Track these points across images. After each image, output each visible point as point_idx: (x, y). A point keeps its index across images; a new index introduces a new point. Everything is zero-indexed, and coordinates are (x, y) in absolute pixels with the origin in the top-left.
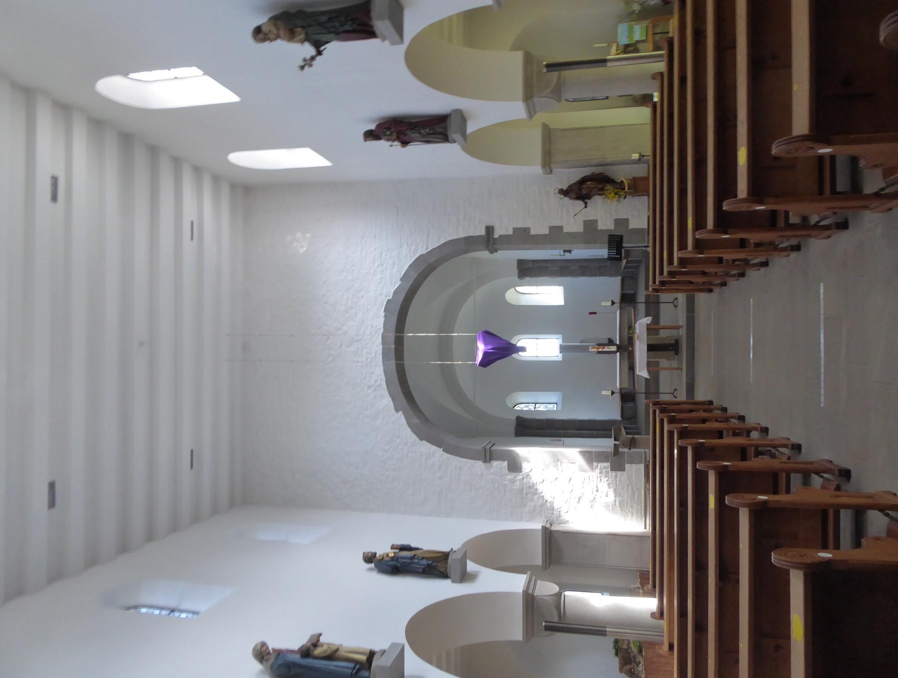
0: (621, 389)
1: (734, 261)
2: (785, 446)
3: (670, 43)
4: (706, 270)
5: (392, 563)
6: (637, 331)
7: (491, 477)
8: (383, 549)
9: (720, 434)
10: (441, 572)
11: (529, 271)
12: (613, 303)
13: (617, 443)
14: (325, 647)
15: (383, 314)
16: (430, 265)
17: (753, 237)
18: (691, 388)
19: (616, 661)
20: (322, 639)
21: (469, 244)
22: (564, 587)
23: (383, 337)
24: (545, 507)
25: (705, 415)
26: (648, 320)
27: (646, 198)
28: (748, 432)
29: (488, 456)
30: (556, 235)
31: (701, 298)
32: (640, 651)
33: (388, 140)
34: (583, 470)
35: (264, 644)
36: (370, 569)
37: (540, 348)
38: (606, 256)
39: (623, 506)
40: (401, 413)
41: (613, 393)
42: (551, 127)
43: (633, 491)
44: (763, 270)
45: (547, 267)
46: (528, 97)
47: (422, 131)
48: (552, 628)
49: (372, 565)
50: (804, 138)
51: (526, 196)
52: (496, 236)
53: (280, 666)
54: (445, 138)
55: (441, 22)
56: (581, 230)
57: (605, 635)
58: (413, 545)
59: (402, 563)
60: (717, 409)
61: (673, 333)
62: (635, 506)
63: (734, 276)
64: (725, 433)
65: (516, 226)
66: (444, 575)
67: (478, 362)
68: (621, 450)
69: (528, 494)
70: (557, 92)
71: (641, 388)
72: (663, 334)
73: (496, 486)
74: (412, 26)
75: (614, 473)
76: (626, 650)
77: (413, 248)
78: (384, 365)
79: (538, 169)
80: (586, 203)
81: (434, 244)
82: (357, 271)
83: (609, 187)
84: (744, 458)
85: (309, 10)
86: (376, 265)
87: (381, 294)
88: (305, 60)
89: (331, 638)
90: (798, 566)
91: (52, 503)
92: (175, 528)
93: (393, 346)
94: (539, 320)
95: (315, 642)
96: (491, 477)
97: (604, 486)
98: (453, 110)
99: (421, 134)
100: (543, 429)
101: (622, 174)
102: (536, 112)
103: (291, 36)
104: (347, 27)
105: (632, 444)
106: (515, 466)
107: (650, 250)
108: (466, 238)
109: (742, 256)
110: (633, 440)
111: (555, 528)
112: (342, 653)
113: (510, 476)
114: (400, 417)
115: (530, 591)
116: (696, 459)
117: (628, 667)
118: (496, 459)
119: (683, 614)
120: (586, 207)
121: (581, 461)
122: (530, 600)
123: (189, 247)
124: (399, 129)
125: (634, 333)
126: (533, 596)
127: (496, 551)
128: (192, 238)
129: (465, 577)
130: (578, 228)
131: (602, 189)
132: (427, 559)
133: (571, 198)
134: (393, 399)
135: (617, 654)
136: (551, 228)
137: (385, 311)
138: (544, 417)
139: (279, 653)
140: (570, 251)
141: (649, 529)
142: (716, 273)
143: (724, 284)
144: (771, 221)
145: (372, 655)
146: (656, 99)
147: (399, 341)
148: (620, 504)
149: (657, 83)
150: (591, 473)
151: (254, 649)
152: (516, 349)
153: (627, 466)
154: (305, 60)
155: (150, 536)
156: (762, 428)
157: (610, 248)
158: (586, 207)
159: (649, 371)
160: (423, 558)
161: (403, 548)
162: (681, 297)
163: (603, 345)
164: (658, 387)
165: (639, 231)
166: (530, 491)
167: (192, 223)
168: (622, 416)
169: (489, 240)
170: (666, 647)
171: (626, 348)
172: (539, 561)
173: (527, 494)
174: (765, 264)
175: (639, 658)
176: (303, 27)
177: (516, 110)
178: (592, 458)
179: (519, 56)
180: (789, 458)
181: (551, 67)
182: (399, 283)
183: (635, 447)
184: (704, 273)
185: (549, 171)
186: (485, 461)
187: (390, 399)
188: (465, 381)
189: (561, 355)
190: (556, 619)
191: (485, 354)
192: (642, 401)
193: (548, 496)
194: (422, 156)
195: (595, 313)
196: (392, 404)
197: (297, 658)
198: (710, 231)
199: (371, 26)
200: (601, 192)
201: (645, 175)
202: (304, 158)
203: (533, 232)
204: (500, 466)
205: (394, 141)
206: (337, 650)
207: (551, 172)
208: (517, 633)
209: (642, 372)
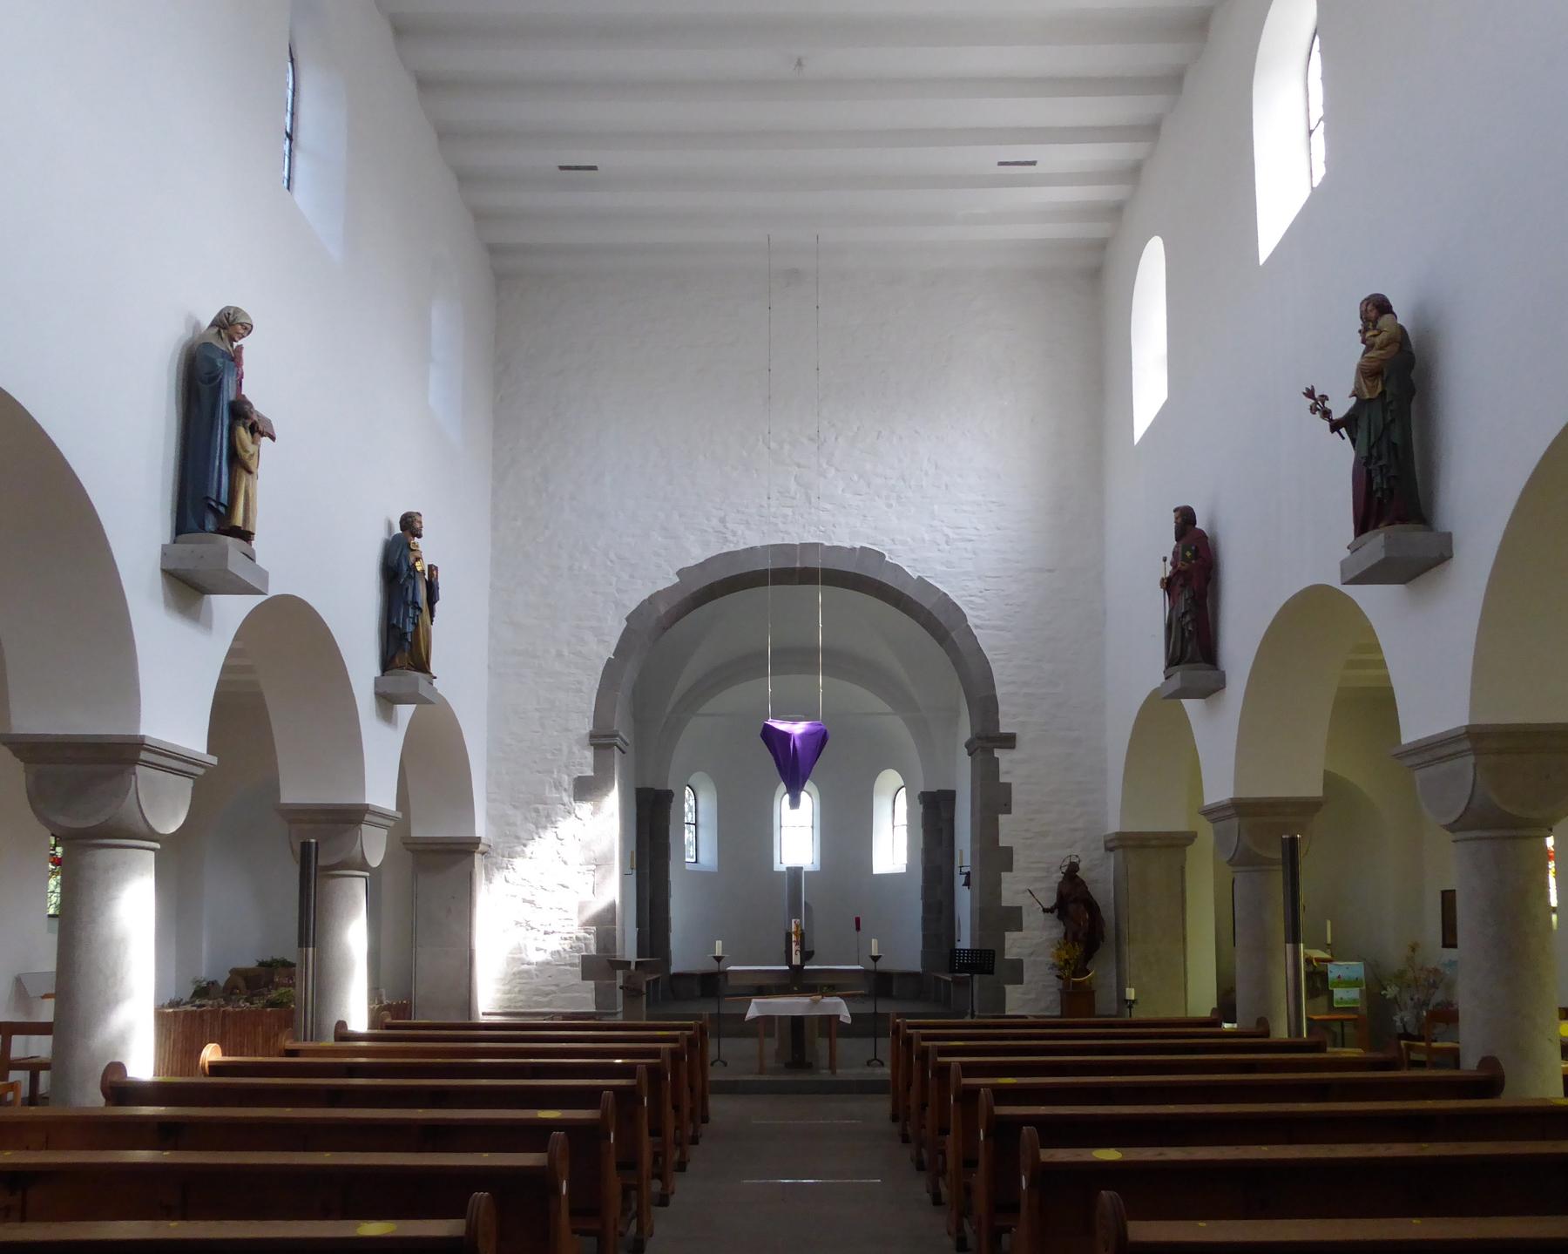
0: (726, 973)
1: (943, 1153)
2: (640, 1229)
3: (1318, 1047)
4: (928, 1109)
5: (405, 568)
6: (827, 1000)
7: (565, 749)
8: (429, 550)
9: (656, 1131)
10: (393, 657)
11: (934, 812)
12: (875, 959)
13: (633, 967)
14: (251, 448)
15: (857, 546)
16: (947, 633)
17: (979, 1179)
18: (731, 1088)
19: (249, 962)
20: (265, 441)
21: (984, 704)
22: (177, 864)
23: (816, 545)
24: (514, 842)
25: (686, 1111)
26: (845, 1015)
27: (1058, 1013)
28: (659, 1176)
29: (601, 741)
30: (995, 858)
31: (881, 1106)
32: (272, 1004)
33: (1175, 553)
34: (581, 909)
35: (248, 329)
36: (390, 527)
37: (797, 835)
38: (959, 946)
39: (522, 976)
41: (718, 959)
42: (1189, 849)
44: (927, 1197)
46: (1239, 808)
47: (1188, 618)
48: (306, 856)
49: (398, 530)
50: (1122, 1235)
51: (1070, 801)
52: (997, 753)
53: (212, 362)
54: (1175, 659)
55: (1377, 648)
57: (300, 945)
58: (437, 605)
59: (405, 588)
60: (695, 1131)
61: (825, 1061)
62: (522, 997)
63: (919, 1154)
64: (658, 1139)
66: (387, 664)
68: (619, 973)
70: (1244, 859)
71: (728, 1007)
72: (822, 1044)
73: (549, 756)
74: (1375, 600)
76: (272, 981)
79: (1114, 825)
80: (1050, 911)
81: (985, 639)
82: (938, 495)
83: (1078, 950)
84: (621, 1166)
85: (1414, 406)
86: (947, 531)
88: (1324, 398)
89: (268, 458)
90: (604, 1116)
92: (446, 134)
94: (846, 831)
95: (259, 429)
96: (565, 749)
97: (555, 944)
98: (1448, 537)
99: (1184, 615)
101: (1100, 974)
102: (1214, 821)
103: (1368, 373)
104: (1377, 480)
105: (631, 992)
106: (586, 789)
107: (968, 1020)
108: (994, 698)
109: (951, 1165)
110: (640, 993)
112: (244, 480)
113: (567, 781)
115: (367, 817)
116: (650, 1068)
117: (241, 984)
118: (595, 756)
119: (353, 1071)
120: (1045, 911)
121: (598, 905)
122: (352, 816)
123: (985, 158)
124: (1195, 571)
125: (824, 995)
126: (361, 822)
127: (434, 757)
128: (1001, 164)
129: (386, 701)
131: (1075, 938)
132: (416, 633)
133: (1061, 884)
134: (701, 566)
135: (262, 964)
136: (1009, 851)
139: (235, 359)
140: (967, 884)
141: (483, 1020)
142: (924, 1127)
143: (905, 1139)
144: (1005, 1205)
145: (246, 535)
146: (1226, 1026)
147: (807, 576)
149: (1251, 1025)
150: (576, 923)
151: (237, 310)
152: (794, 790)
153: (591, 984)
154: (1324, 398)
155: (426, 84)
156: (667, 1196)
157: (971, 951)
158: (1045, 911)
159: (756, 1020)
160: (416, 625)
162: (885, 1072)
163: (802, 943)
164: (729, 1036)
165: (1001, 1001)
166: (541, 816)
167: (1033, 163)
168: (678, 976)
169: (990, 741)
170: (289, 1044)
171: (796, 981)
172: (417, 832)
173: (537, 811)
174: (937, 1200)
175: (259, 1003)
176: (1383, 393)
177: (1219, 788)
178: (603, 923)
179: (1315, 790)
180: (622, 1235)
181: (1291, 847)
183: (625, 996)
184: (924, 1106)
185: (1111, 845)
186: (592, 736)
188: (734, 698)
189: (783, 868)
190: (321, 862)
191: (786, 736)
192: (706, 1009)
193: (532, 847)
194: (1144, 616)
195: (858, 928)
196: (692, 563)
197: (229, 394)
198: (990, 1110)
199: (1376, 527)
200: (1070, 938)
201: (1097, 1012)
202: (1149, 390)
203: (1002, 818)
204: (585, 761)
205: (1174, 564)
206: (250, 472)
207: (1109, 849)
208: (291, 794)
209: (755, 1008)
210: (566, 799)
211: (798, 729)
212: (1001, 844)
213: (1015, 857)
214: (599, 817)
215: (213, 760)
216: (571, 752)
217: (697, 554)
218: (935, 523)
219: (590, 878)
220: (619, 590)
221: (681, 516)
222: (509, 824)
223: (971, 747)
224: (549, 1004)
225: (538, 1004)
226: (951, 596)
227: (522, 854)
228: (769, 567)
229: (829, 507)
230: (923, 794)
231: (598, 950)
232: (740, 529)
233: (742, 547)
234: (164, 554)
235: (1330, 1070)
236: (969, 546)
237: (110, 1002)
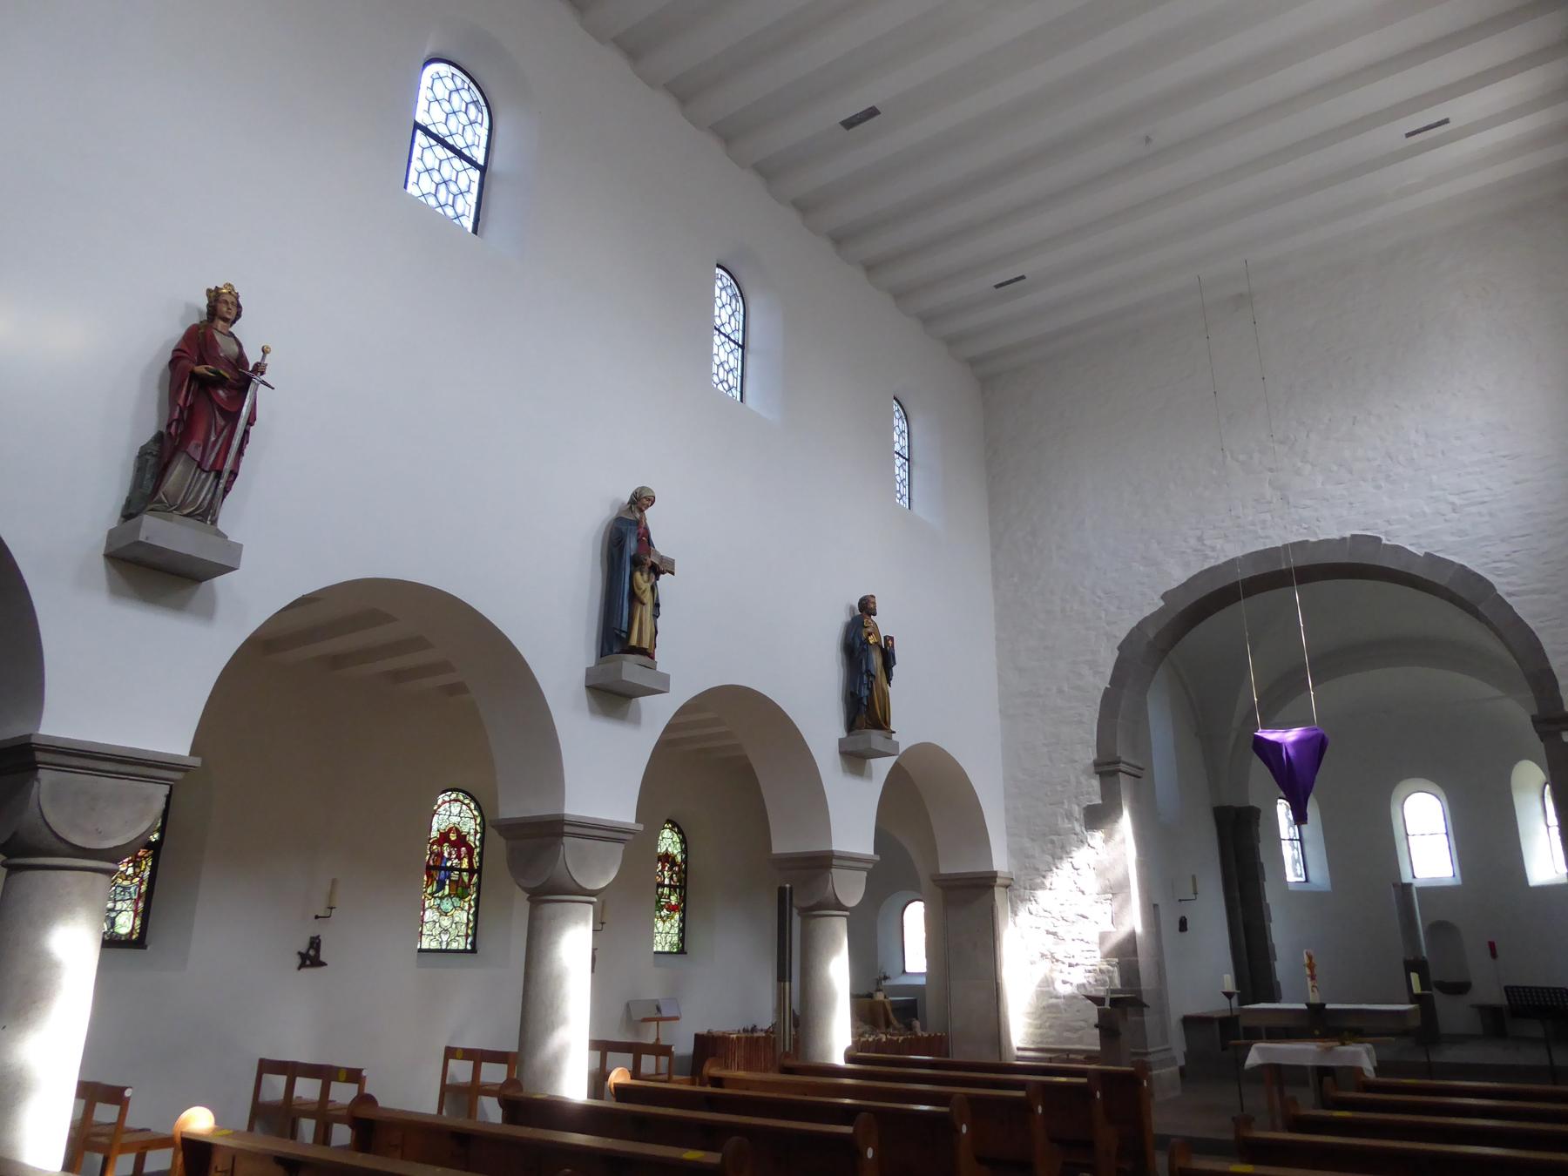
5: (858, 642)
7: (1073, 779)
8: (884, 623)
15: (1348, 534)
29: (1106, 769)
35: (652, 501)
39: (1050, 1009)
43: (1076, 1030)
48: (783, 901)
59: (865, 658)
62: (1053, 1033)
66: (851, 725)
69: (1051, 846)
91: (849, 124)
96: (1073, 779)
106: (1098, 817)
108: (1550, 671)
111: (999, 893)
113: (1077, 811)
114: (1154, 604)
115: (835, 862)
121: (1119, 934)
122: (821, 863)
126: (830, 866)
128: (1408, 135)
129: (854, 759)
134: (1184, 586)
137: (1354, 536)
138: (1264, 856)
145: (648, 653)
148: (1053, 1006)
150: (1098, 954)
151: (643, 488)
155: (871, 268)
160: (871, 690)
161: (888, 659)
166: (1057, 848)
167: (1446, 121)
173: (1052, 842)
182: (1421, 553)
186: (1097, 764)
191: (1276, 746)
195: (1494, 954)
196: (1175, 585)
210: (1078, 828)
211: (1290, 736)
214: (1112, 844)
215: (640, 827)
216: (1079, 783)
217: (1178, 575)
218: (1435, 493)
219: (1108, 908)
222: (1028, 857)
224: (1080, 1040)
225: (1069, 1040)
227: (1042, 886)
228: (1240, 578)
229: (1308, 502)
232: (1219, 544)
233: (1222, 560)
234: (588, 676)
235: (1384, 1111)
237: (549, 1027)
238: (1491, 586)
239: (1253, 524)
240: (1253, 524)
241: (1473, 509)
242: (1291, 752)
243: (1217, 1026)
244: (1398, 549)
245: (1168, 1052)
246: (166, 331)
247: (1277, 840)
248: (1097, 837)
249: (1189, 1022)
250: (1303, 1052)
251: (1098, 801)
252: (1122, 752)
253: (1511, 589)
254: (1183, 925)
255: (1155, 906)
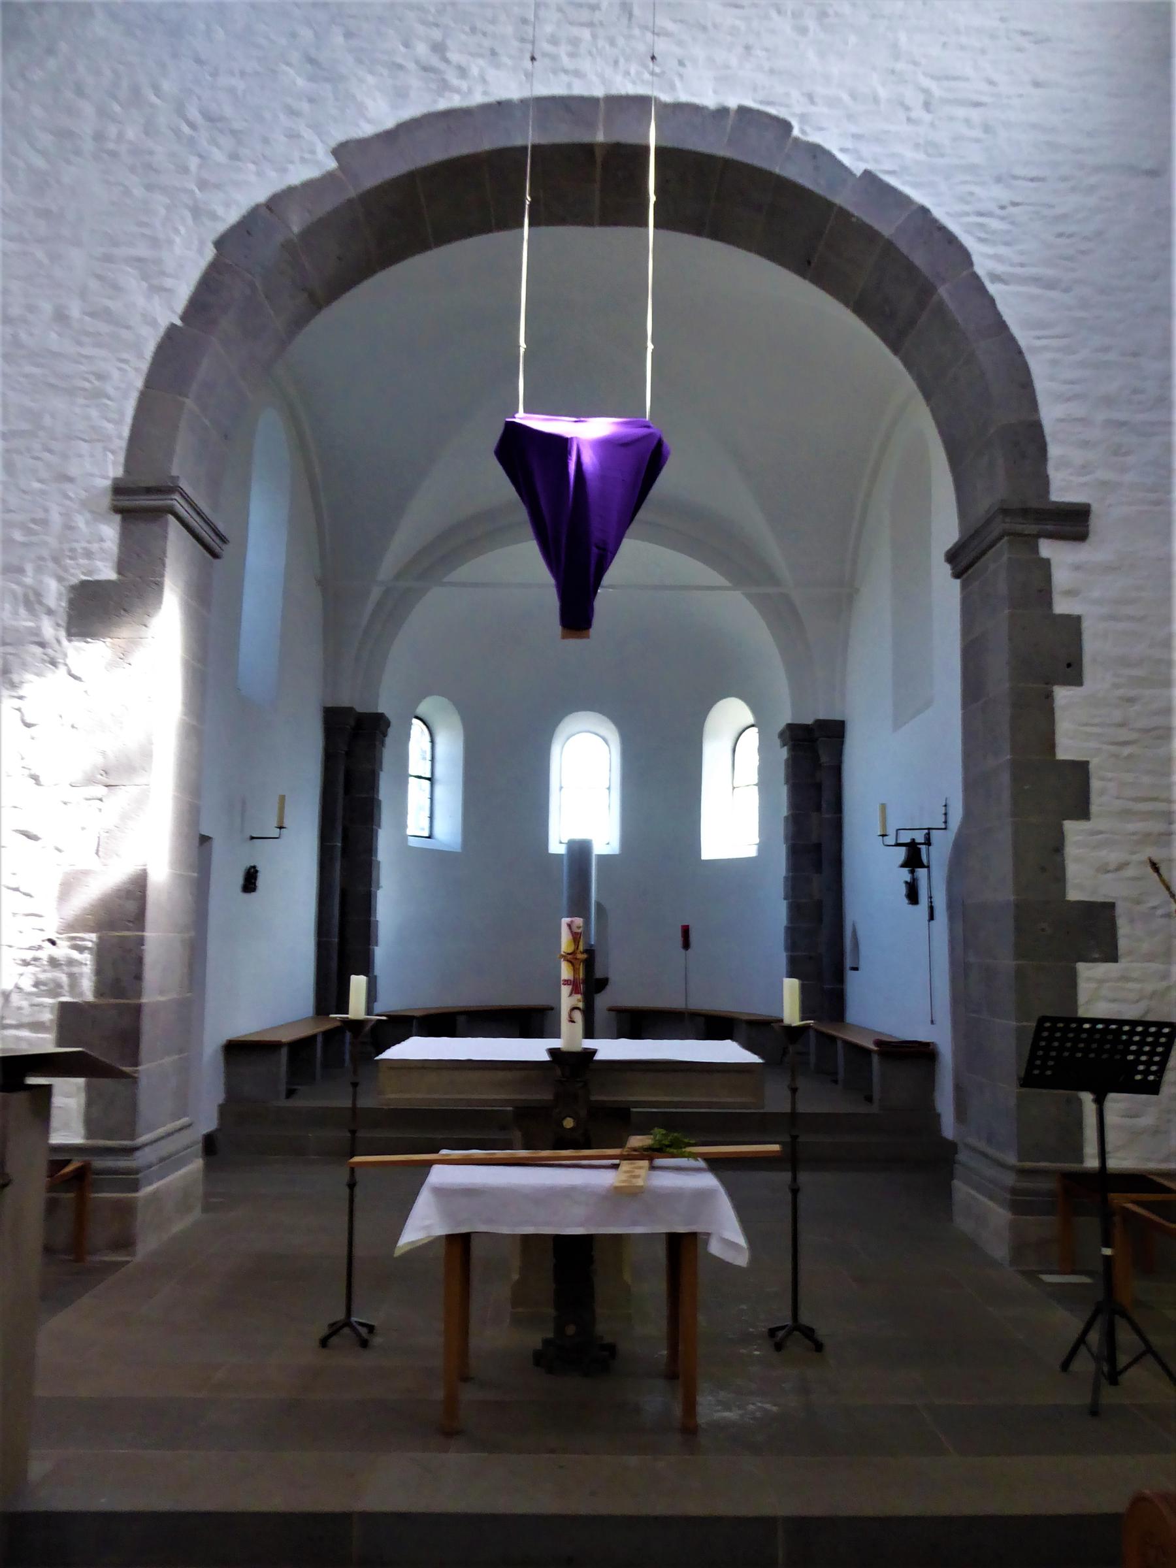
7: (56, 518)
15: (732, 103)
29: (139, 503)
34: (67, 888)
37: (585, 791)
40: (332, 164)
45: (818, 808)
52: (1047, 549)
56: (1074, 895)
65: (1086, 625)
67: (520, 417)
75: (48, 1016)
77: (995, 224)
78: (524, 102)
81: (1011, 304)
86: (926, 83)
87: (811, 98)
93: (600, 138)
94: (662, 780)
96: (56, 518)
100: (347, 791)
106: (96, 609)
113: (54, 592)
118: (125, 537)
121: (107, 878)
130: (1083, 881)
136: (1081, 769)
137: (743, 111)
171: (568, 1110)
182: (858, 168)
186: (119, 489)
187: (389, 123)
191: (561, 444)
195: (686, 945)
196: (367, 130)
203: (1062, 694)
204: (100, 549)
210: (49, 629)
212: (1062, 755)
213: (1095, 784)
216: (69, 527)
218: (900, 66)
220: (203, 185)
221: (349, 35)
223: (962, 560)
226: (938, 213)
229: (670, 26)
230: (791, 727)
231: (99, 991)
233: (478, 98)
236: (975, 114)
238: (965, 257)
239: (554, 41)
240: (554, 41)
241: (961, 112)
242: (588, 459)
243: (284, 1051)
244: (817, 152)
245: (181, 1101)
246: (80, 866)
247: (402, 777)
248: (87, 655)
249: (237, 1051)
250: (560, 1191)
251: (107, 572)
252: (182, 467)
253: (1000, 268)
254: (250, 881)
255: (204, 840)
